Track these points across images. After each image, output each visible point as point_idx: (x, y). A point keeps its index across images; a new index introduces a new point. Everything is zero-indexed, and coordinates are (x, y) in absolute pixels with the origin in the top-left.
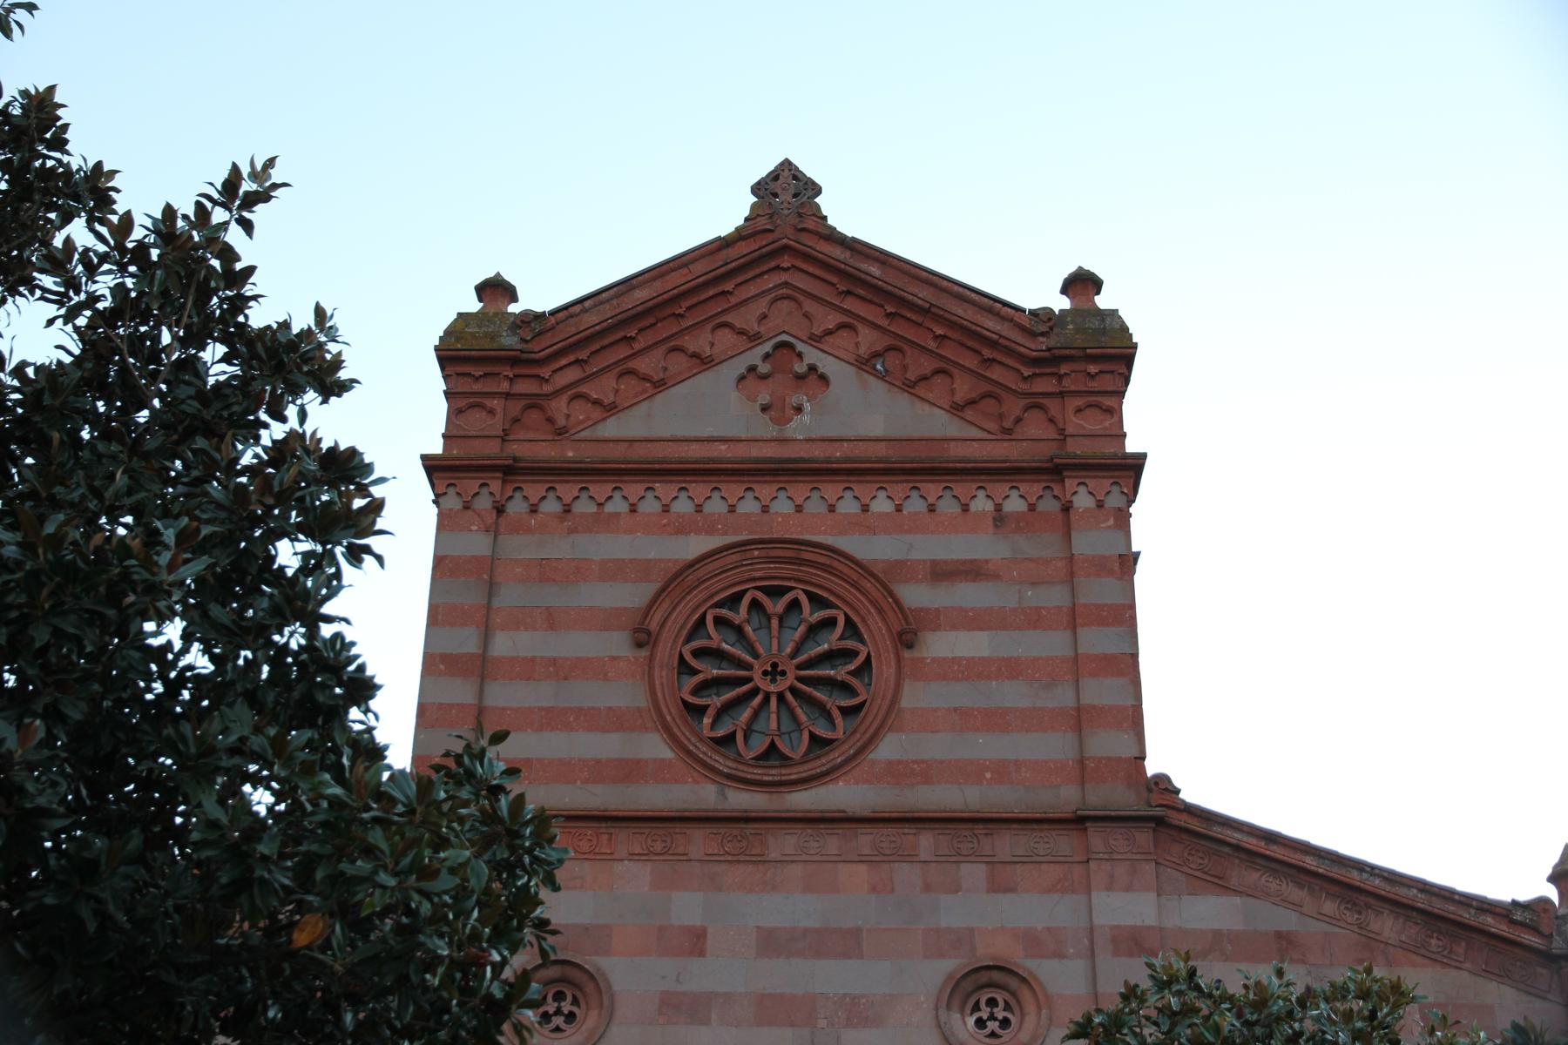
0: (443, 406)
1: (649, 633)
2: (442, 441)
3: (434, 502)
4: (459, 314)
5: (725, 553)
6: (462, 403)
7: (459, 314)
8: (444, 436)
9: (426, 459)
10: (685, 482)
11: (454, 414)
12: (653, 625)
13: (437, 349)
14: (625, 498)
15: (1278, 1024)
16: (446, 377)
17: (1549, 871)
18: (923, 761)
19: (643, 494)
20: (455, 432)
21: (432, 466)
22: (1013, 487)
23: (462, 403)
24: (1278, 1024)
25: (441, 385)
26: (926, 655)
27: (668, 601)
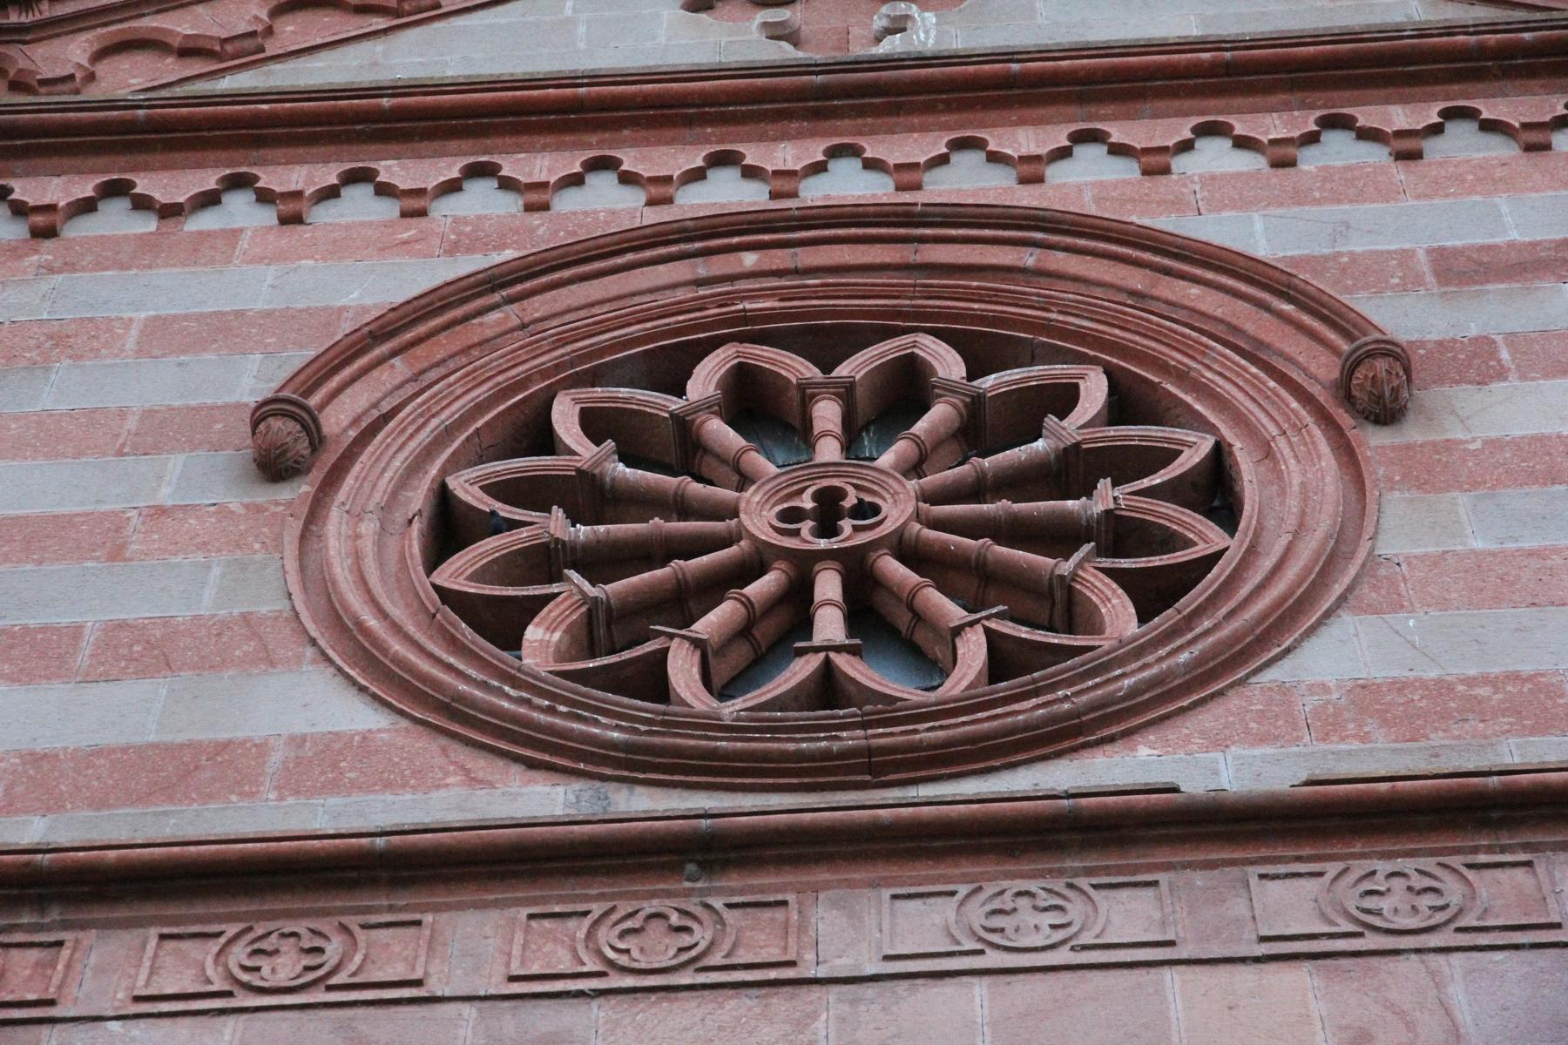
1: (317, 440)
5: (630, 257)
12: (338, 418)
18: (1515, 677)
26: (1459, 435)
27: (400, 368)
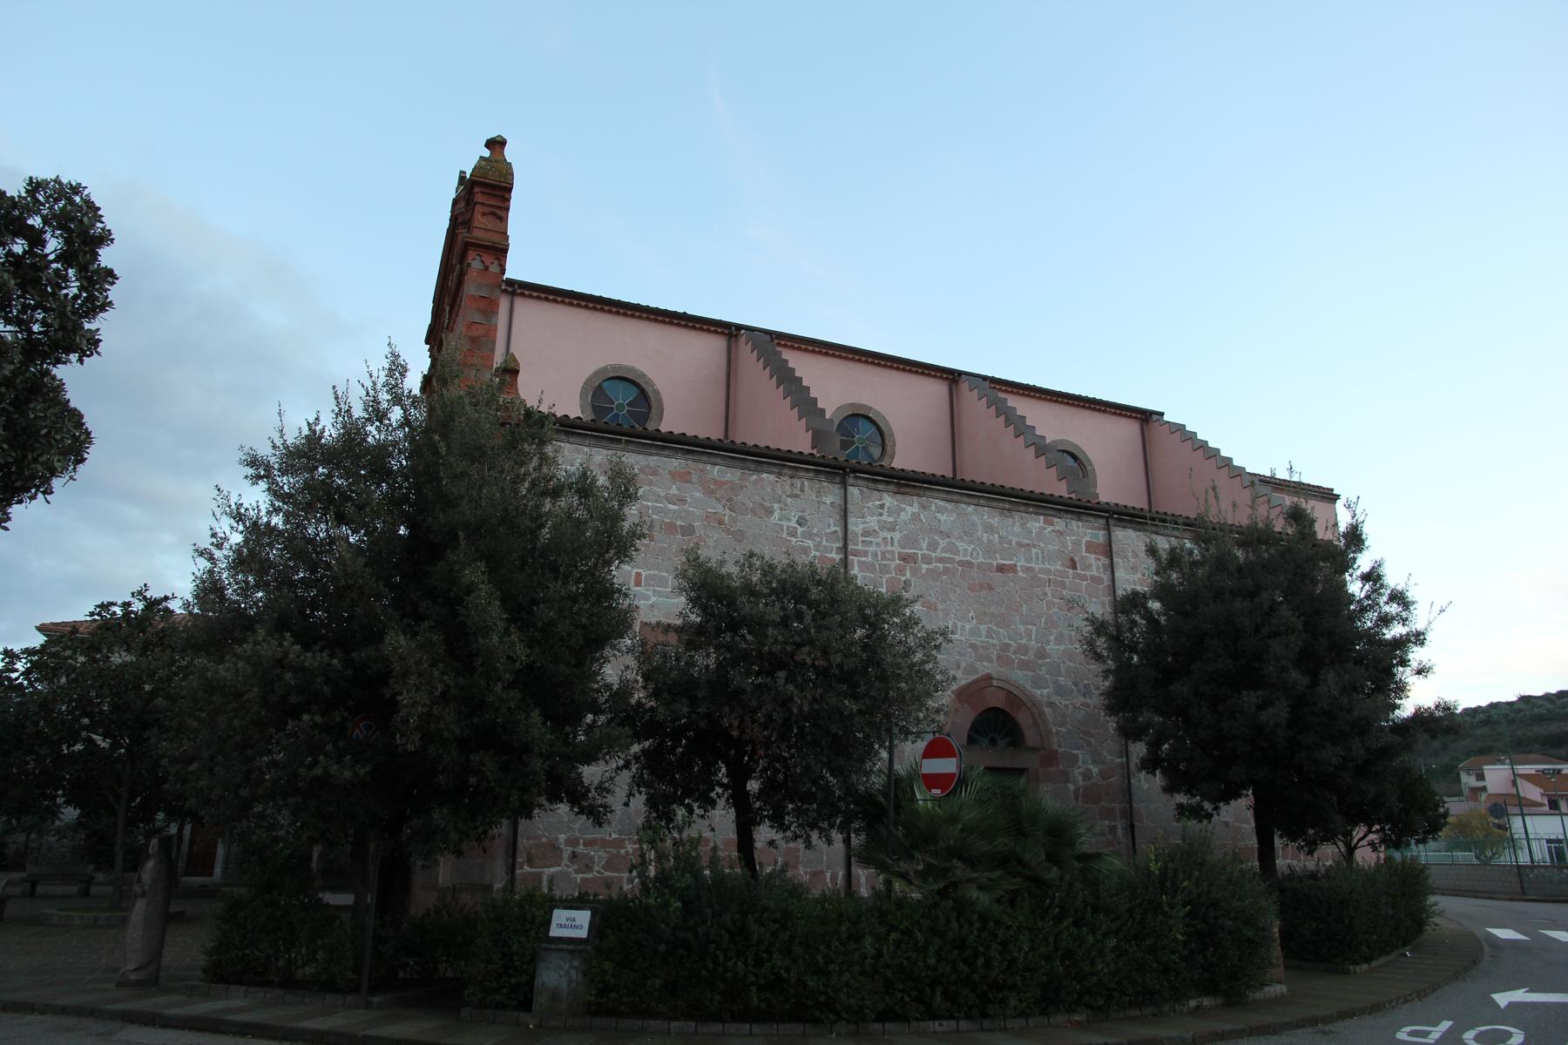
14: (482, 262)
22: (478, 255)
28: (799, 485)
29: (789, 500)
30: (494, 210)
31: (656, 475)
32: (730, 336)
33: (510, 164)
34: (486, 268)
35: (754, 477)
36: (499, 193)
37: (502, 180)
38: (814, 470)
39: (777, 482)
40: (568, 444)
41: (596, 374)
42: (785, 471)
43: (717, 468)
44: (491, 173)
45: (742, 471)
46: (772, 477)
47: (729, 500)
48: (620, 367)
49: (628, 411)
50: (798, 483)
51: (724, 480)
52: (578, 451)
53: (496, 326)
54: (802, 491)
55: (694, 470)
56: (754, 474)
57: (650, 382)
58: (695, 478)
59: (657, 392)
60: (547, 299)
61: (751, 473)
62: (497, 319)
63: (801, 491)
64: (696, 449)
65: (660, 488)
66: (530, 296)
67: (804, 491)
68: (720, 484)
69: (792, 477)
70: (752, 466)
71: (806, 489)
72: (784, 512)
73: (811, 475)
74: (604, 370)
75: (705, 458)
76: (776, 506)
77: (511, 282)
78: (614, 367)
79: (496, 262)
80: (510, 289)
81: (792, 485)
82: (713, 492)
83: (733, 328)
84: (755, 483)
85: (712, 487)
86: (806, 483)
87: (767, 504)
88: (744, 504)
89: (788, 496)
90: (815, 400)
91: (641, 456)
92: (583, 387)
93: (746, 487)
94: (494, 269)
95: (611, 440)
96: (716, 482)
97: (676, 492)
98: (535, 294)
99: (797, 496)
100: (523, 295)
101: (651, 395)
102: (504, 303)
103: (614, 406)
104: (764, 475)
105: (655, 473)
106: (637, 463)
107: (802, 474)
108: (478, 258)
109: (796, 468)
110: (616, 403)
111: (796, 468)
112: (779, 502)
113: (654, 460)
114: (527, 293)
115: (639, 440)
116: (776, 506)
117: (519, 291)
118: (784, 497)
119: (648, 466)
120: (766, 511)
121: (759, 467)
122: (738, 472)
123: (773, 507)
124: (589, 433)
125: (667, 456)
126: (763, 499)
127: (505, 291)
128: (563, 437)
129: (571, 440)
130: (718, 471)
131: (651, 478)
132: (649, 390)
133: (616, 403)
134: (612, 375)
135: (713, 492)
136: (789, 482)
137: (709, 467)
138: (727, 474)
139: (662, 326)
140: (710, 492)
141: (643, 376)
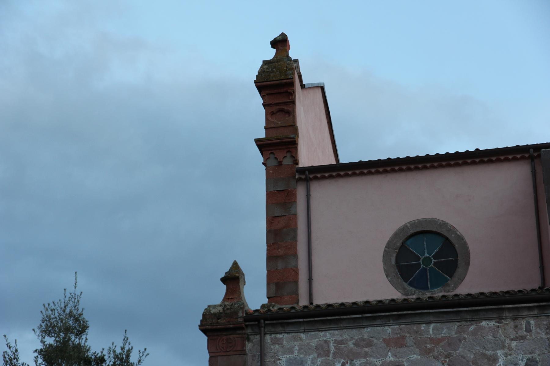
0: (263, 111)
2: (264, 131)
3: (264, 164)
4: (264, 61)
6: (274, 109)
7: (264, 61)
8: (265, 128)
9: (257, 141)
10: (273, 150)
11: (269, 115)
13: (256, 82)
14: (276, 158)
15: (347, 339)
16: (263, 97)
17: (223, 275)
19: (286, 155)
20: (269, 126)
21: (261, 144)
22: (271, 153)
23: (274, 109)
24: (347, 339)
25: (261, 101)
28: (524, 326)
29: (514, 344)
30: (280, 107)
31: (371, 345)
32: (532, 159)
33: (291, 58)
34: (280, 164)
35: (472, 328)
36: (282, 90)
37: (283, 77)
38: (537, 307)
39: (498, 327)
40: (286, 335)
41: (396, 235)
42: (505, 314)
43: (432, 326)
44: (272, 74)
45: (458, 324)
46: (492, 324)
47: (448, 356)
48: (420, 222)
49: (435, 264)
50: (523, 323)
51: (440, 337)
52: (295, 339)
53: (295, 215)
54: (528, 330)
55: (409, 333)
56: (472, 325)
57: (452, 230)
58: (409, 341)
59: (460, 238)
60: (339, 176)
61: (469, 323)
62: (296, 208)
63: (526, 331)
64: (405, 312)
65: (376, 357)
66: (324, 178)
67: (531, 331)
68: (436, 342)
69: (514, 319)
70: (468, 317)
71: (533, 328)
72: (509, 357)
73: (536, 312)
74: (404, 229)
75: (417, 319)
76: (499, 352)
77: (303, 170)
78: (413, 224)
79: (288, 155)
80: (303, 177)
81: (516, 327)
82: (431, 350)
83: (532, 150)
84: (474, 333)
85: (429, 346)
86: (532, 322)
87: (490, 353)
88: (464, 358)
89: (512, 340)
90: (201, 321)
91: (354, 330)
92: (385, 250)
93: (465, 339)
94: (287, 161)
95: (323, 322)
96: (432, 340)
97: (392, 359)
98: (327, 175)
99: (523, 338)
100: (316, 178)
101: (454, 241)
102: (301, 192)
103: (421, 262)
104: (484, 323)
105: (369, 344)
106: (352, 338)
107: (526, 313)
108: (272, 156)
109: (517, 309)
110: (422, 258)
111: (517, 309)
112: (503, 348)
113: (367, 332)
114: (319, 175)
115: (349, 317)
116: (499, 352)
117: (311, 176)
118: (508, 341)
119: (363, 339)
120: (489, 359)
121: (476, 317)
122: (455, 326)
123: (496, 355)
124: (301, 320)
125: (380, 325)
126: (485, 348)
127: (300, 179)
128: (280, 329)
129: (288, 330)
130: (433, 329)
131: (366, 349)
132: (452, 237)
133: (422, 258)
134: (412, 232)
135: (431, 350)
136: (512, 324)
137: (423, 327)
138: (442, 329)
139: (458, 170)
140: (426, 352)
141: (444, 224)
